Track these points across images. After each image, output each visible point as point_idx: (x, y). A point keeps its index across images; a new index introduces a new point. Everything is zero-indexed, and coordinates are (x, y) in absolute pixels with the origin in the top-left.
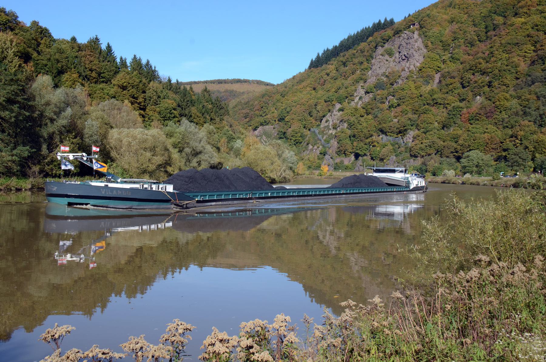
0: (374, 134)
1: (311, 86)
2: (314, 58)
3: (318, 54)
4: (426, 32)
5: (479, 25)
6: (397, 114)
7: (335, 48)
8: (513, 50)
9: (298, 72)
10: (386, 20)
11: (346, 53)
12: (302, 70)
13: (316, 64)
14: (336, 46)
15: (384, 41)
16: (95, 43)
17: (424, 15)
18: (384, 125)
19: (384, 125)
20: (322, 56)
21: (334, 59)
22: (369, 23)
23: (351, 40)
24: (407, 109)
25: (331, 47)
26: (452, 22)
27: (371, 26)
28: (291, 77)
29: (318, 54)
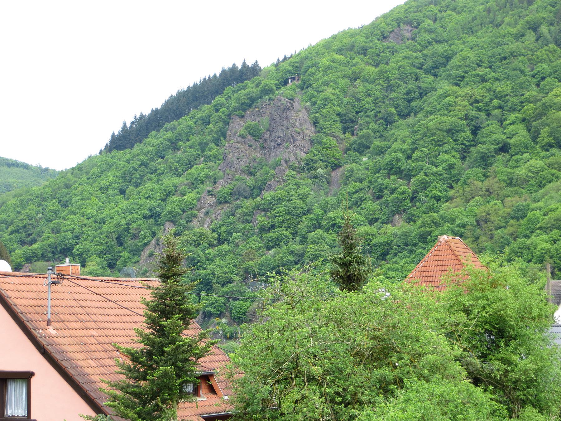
0: (235, 278)
1: (116, 186)
2: (117, 130)
3: (125, 124)
4: (314, 96)
5: (398, 88)
6: (271, 244)
7: (155, 113)
8: (445, 141)
9: (85, 157)
10: (244, 64)
11: (175, 123)
12: (95, 152)
13: (121, 142)
14: (157, 110)
15: (244, 107)
16: (152, 111)
17: (309, 63)
18: (251, 263)
19: (251, 263)
20: (131, 127)
21: (154, 133)
22: (214, 69)
23: (184, 100)
24: (287, 233)
25: (147, 112)
26: (356, 80)
27: (185, 89)
28: (74, 165)
29: (125, 124)
